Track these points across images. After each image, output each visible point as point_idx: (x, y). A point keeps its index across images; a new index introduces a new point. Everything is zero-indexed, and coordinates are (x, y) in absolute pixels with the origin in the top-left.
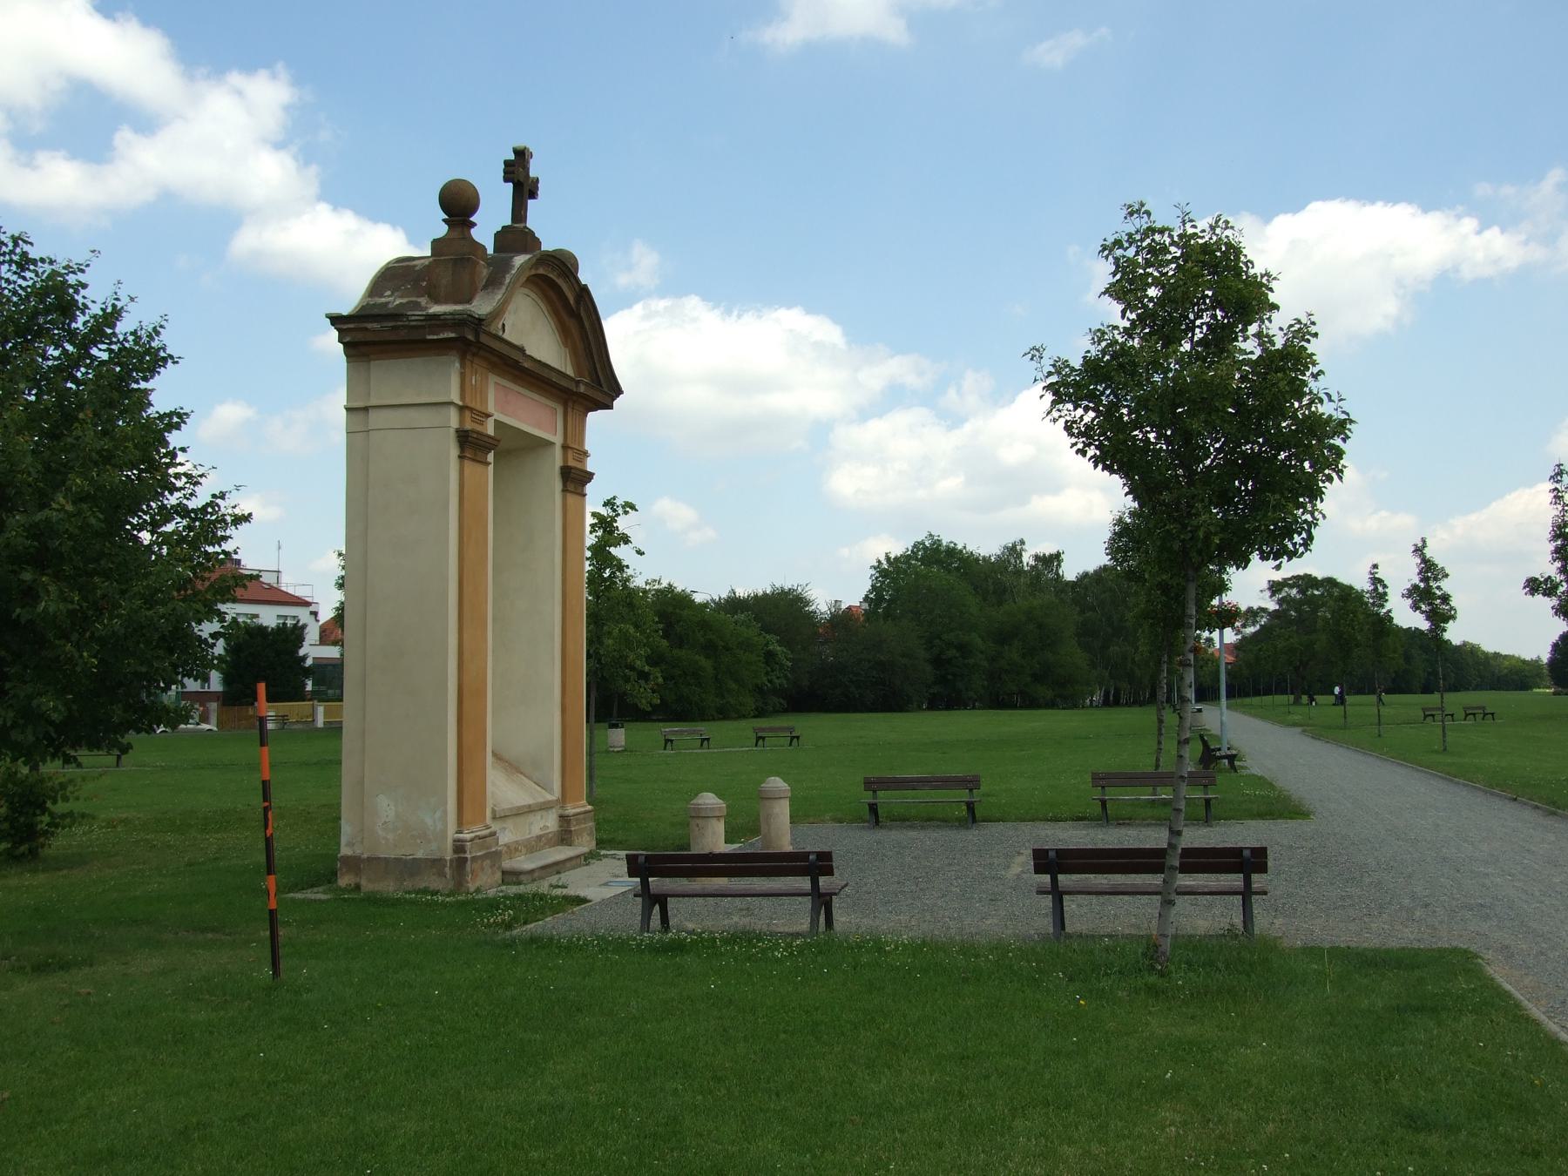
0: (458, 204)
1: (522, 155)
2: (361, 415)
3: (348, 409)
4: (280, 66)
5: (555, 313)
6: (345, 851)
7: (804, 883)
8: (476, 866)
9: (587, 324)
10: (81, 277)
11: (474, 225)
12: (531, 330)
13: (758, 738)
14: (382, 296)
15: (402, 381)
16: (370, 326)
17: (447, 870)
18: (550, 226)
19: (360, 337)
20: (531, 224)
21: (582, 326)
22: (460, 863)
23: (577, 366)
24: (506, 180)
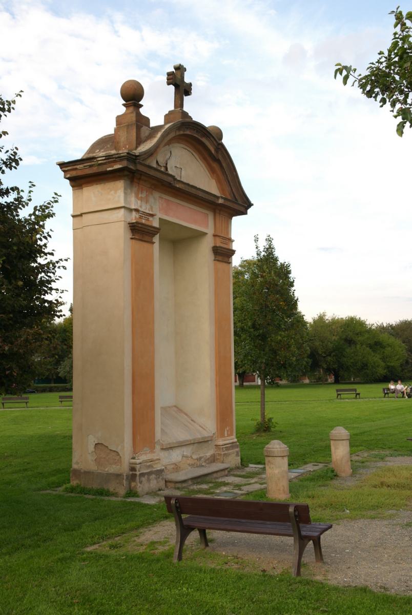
0: (133, 95)
1: (180, 69)
2: (79, 218)
3: (73, 216)
4: (327, 321)
5: (204, 159)
6: (75, 466)
7: (355, 392)
8: (143, 479)
9: (224, 165)
10: (22, 208)
11: (141, 106)
12: (186, 167)
13: (338, 395)
14: (94, 153)
15: (96, 195)
16: (78, 167)
17: (124, 482)
18: (199, 110)
19: (74, 174)
20: (185, 109)
21: (222, 167)
22: (132, 477)
23: (222, 190)
24: (169, 84)
